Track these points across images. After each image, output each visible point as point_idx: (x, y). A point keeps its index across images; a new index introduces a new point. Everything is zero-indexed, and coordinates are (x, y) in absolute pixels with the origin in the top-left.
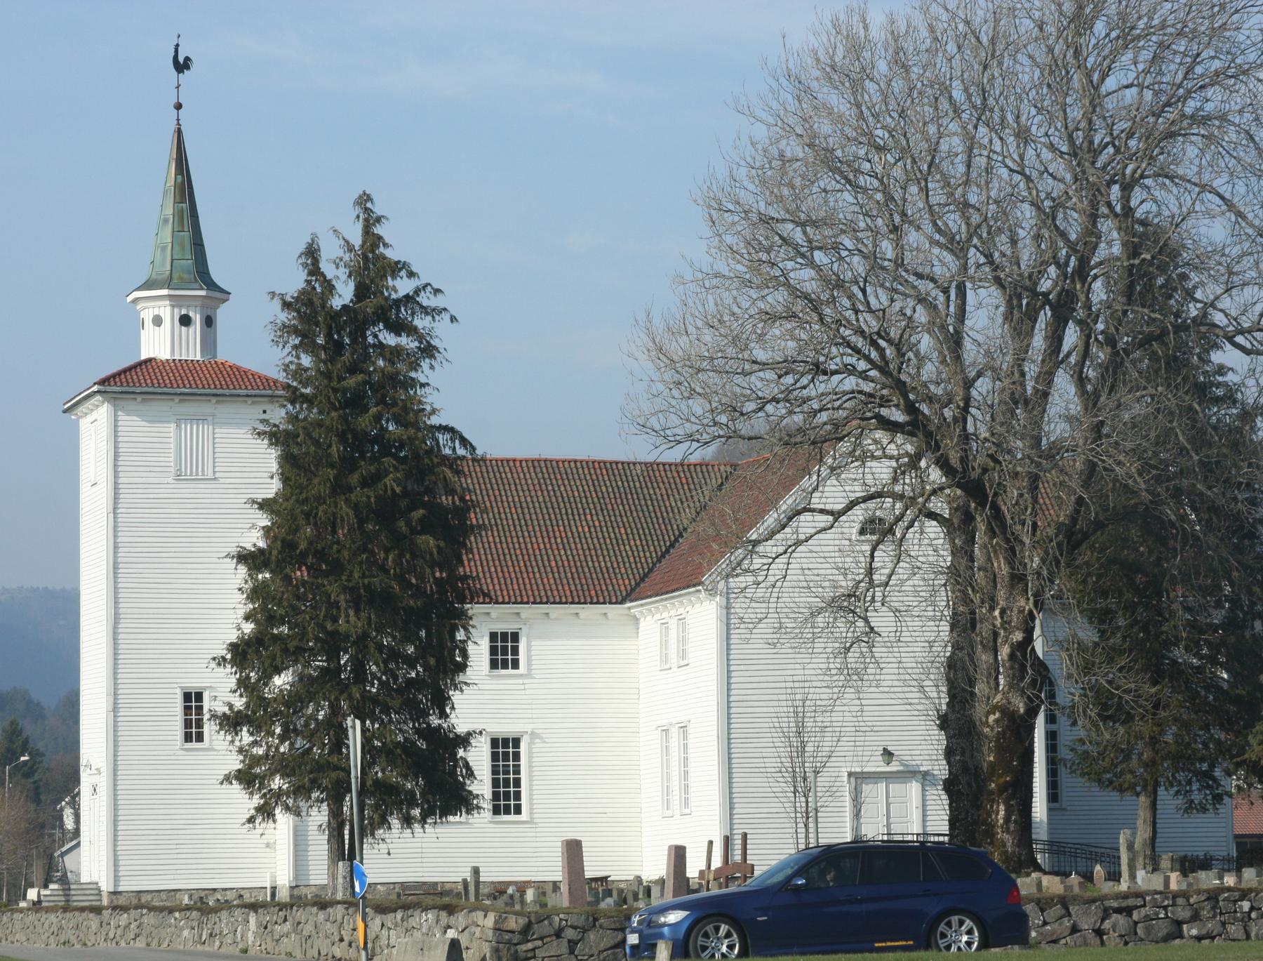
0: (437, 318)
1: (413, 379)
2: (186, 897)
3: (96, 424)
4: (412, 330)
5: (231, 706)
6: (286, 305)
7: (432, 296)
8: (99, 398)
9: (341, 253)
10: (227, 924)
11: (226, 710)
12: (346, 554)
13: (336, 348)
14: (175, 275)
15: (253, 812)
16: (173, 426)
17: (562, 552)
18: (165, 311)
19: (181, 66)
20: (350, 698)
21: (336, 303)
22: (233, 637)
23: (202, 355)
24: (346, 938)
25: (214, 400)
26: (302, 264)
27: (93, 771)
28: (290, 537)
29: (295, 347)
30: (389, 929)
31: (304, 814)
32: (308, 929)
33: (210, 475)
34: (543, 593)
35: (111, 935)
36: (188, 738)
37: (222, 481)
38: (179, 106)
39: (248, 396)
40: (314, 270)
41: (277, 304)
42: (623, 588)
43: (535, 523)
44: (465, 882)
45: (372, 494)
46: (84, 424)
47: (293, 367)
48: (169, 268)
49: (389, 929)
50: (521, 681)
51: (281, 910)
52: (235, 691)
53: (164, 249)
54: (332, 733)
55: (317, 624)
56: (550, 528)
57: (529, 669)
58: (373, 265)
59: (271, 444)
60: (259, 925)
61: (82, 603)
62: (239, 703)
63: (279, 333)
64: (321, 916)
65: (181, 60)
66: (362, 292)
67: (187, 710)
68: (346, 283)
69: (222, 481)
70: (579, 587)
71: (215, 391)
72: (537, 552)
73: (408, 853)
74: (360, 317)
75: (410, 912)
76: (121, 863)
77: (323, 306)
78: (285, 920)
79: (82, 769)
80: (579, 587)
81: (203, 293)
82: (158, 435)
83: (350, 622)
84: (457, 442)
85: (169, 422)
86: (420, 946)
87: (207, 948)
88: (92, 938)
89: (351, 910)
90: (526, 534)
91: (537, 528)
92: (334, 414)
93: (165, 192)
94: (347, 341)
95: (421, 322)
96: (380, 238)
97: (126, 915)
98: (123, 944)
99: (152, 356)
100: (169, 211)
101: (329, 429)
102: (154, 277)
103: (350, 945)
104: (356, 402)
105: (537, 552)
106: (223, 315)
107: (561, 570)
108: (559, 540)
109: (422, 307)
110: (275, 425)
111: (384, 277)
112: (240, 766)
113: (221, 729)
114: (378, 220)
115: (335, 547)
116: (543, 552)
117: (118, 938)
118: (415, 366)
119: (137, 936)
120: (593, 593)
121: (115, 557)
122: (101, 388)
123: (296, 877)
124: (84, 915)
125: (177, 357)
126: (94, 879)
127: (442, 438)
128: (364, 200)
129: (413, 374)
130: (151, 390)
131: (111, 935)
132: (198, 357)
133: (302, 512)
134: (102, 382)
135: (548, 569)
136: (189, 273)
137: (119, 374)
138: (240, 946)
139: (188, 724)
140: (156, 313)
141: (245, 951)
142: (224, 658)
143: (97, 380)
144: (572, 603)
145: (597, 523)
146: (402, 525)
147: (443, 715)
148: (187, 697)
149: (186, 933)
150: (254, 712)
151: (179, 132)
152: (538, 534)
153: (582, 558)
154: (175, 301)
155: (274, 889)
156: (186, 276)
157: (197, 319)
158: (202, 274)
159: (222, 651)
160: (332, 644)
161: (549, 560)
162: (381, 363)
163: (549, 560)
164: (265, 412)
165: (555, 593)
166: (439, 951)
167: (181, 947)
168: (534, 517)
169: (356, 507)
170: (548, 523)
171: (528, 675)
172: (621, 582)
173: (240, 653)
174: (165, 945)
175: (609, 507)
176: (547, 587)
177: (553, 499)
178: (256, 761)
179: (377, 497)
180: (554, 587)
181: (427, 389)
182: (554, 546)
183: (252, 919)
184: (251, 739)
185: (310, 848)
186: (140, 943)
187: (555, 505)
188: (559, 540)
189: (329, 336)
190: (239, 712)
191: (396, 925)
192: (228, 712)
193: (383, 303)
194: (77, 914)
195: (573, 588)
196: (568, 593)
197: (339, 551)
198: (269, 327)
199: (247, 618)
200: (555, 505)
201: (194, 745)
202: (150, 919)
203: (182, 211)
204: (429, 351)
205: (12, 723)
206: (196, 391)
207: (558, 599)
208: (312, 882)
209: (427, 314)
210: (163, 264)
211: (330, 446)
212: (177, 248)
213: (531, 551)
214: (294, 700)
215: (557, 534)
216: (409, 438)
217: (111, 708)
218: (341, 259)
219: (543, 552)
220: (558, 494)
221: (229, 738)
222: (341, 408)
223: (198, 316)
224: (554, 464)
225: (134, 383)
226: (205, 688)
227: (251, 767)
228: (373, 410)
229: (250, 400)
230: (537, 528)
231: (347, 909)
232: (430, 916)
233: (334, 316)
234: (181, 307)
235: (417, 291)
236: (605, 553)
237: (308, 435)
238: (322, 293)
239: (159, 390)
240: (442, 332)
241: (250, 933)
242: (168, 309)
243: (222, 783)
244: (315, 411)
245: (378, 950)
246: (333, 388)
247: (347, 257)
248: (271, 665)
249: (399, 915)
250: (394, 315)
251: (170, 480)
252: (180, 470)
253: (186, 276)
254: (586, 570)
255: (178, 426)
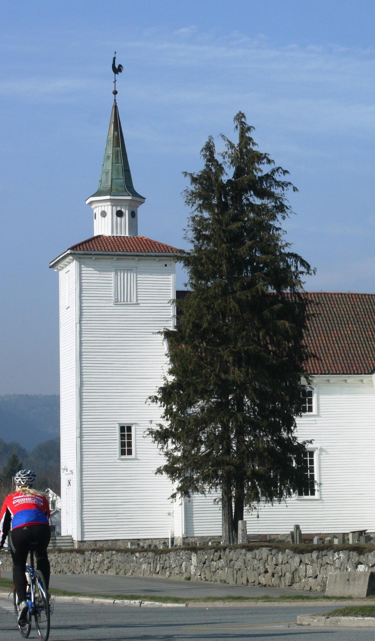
0: (285, 188)
1: (271, 225)
2: (129, 544)
3: (69, 274)
4: (271, 195)
5: (161, 426)
6: (194, 180)
7: (282, 175)
8: (71, 257)
9: (226, 149)
10: (175, 561)
11: (158, 428)
12: (232, 331)
13: (223, 207)
14: (114, 188)
15: (175, 491)
16: (113, 274)
17: (336, 345)
18: (108, 208)
19: (117, 70)
20: (236, 420)
21: (225, 179)
22: (162, 384)
23: (129, 234)
24: (270, 571)
25: (137, 258)
26: (204, 155)
27: (69, 472)
28: (198, 321)
29: (200, 205)
30: (307, 564)
31: (207, 493)
32: (239, 564)
33: (135, 302)
34: (326, 368)
35: (91, 567)
36: (123, 453)
37: (141, 305)
38: (115, 93)
39: (156, 256)
40: (211, 159)
41: (188, 179)
42: (371, 365)
43: (320, 329)
44: (292, 533)
45: (249, 295)
46: (62, 274)
47: (197, 219)
48: (110, 183)
49: (307, 564)
50: (313, 419)
51: (216, 551)
52: (164, 417)
53: (107, 173)
54: (225, 443)
55: (215, 375)
56: (328, 332)
57: (318, 412)
58: (246, 156)
59: (186, 265)
60: (199, 561)
61: (61, 376)
62: (166, 424)
63: (190, 197)
64: (249, 555)
65: (117, 66)
66: (238, 174)
67: (122, 436)
68: (229, 167)
69: (141, 305)
70: (347, 365)
71: (137, 253)
72: (322, 345)
73: (269, 517)
74: (239, 187)
75: (324, 553)
76: (85, 524)
77: (217, 180)
78: (220, 558)
79: (62, 471)
80: (347, 365)
81: (130, 198)
82: (105, 280)
83: (236, 374)
84: (299, 263)
85: (111, 271)
86: (347, 577)
87: (160, 576)
88: (79, 569)
89: (274, 552)
90: (315, 335)
91: (321, 332)
92: (224, 245)
93: (108, 141)
94: (230, 202)
95: (277, 191)
96: (250, 139)
97: (101, 555)
98: (99, 573)
99: (101, 234)
100: (110, 152)
101: (221, 255)
102: (101, 189)
103: (273, 575)
104: (235, 239)
105: (322, 345)
106: (141, 210)
107: (336, 355)
108: (334, 339)
109: (276, 182)
110: (188, 254)
111: (253, 163)
112: (167, 463)
113: (156, 440)
114: (249, 129)
115: (225, 328)
116: (325, 345)
117: (96, 569)
118: (274, 217)
119: (109, 568)
120: (355, 368)
121: (81, 349)
122: (72, 251)
123: (186, 532)
124: (73, 554)
125: (115, 235)
126: (69, 534)
127: (290, 261)
128: (240, 117)
129: (271, 223)
130: (100, 253)
131: (91, 567)
132: (127, 235)
133: (205, 306)
134: (73, 248)
135: (329, 355)
136: (122, 187)
137: (82, 244)
138: (185, 575)
139: (123, 445)
140: (103, 209)
141: (189, 579)
142: (156, 398)
143: (70, 247)
144: (343, 374)
145: (355, 329)
146: (266, 313)
147: (290, 431)
148: (122, 429)
149: (144, 566)
150: (176, 430)
151: (116, 107)
152: (322, 335)
153: (348, 348)
154: (114, 203)
155: (173, 539)
156: (120, 188)
157: (127, 213)
158: (129, 187)
159: (155, 393)
160: (224, 388)
161: (329, 350)
162: (252, 215)
163: (329, 350)
164: (166, 265)
165: (333, 368)
166: (361, 582)
167: (142, 576)
168: (319, 325)
169: (239, 301)
170: (328, 329)
171: (318, 416)
172: (370, 362)
173: (167, 394)
174: (129, 574)
175: (362, 320)
176: (328, 365)
177: (330, 315)
178: (176, 460)
179: (253, 297)
180: (332, 365)
181: (280, 232)
182: (331, 342)
183: (194, 558)
184: (174, 446)
185: (195, 515)
186: (112, 573)
187: (331, 319)
188: (334, 339)
189: (219, 199)
190: (167, 429)
191: (312, 562)
192: (160, 430)
193: (253, 178)
194: (68, 554)
195: (343, 365)
196: (340, 368)
197: (227, 330)
198: (184, 194)
199: (171, 372)
200: (331, 319)
201: (127, 457)
202: (118, 557)
203: (117, 152)
204: (281, 208)
205: (14, 456)
206: (126, 253)
207: (335, 372)
208: (195, 535)
209: (279, 186)
210: (107, 182)
211: (221, 266)
212: (115, 173)
213: (318, 345)
214: (202, 422)
215: (333, 335)
216: (271, 261)
217: (78, 435)
218: (226, 153)
219: (325, 345)
220: (333, 312)
221: (160, 446)
222: (227, 242)
223: (127, 211)
224: (330, 295)
225: (91, 250)
226: (133, 424)
227: (174, 463)
228: (248, 243)
229: (157, 259)
230: (321, 332)
231: (270, 550)
232: (341, 555)
233: (222, 186)
234: (117, 206)
235: (273, 172)
236: (361, 346)
237: (208, 258)
238: (216, 172)
239: (105, 253)
240: (289, 197)
241: (192, 567)
242: (110, 207)
243: (156, 473)
244: (211, 244)
245: (297, 579)
246: (223, 230)
247: (230, 152)
248: (187, 400)
249: (315, 554)
250: (262, 187)
251: (112, 305)
252: (117, 299)
253: (120, 188)
254: (350, 355)
255: (116, 274)
